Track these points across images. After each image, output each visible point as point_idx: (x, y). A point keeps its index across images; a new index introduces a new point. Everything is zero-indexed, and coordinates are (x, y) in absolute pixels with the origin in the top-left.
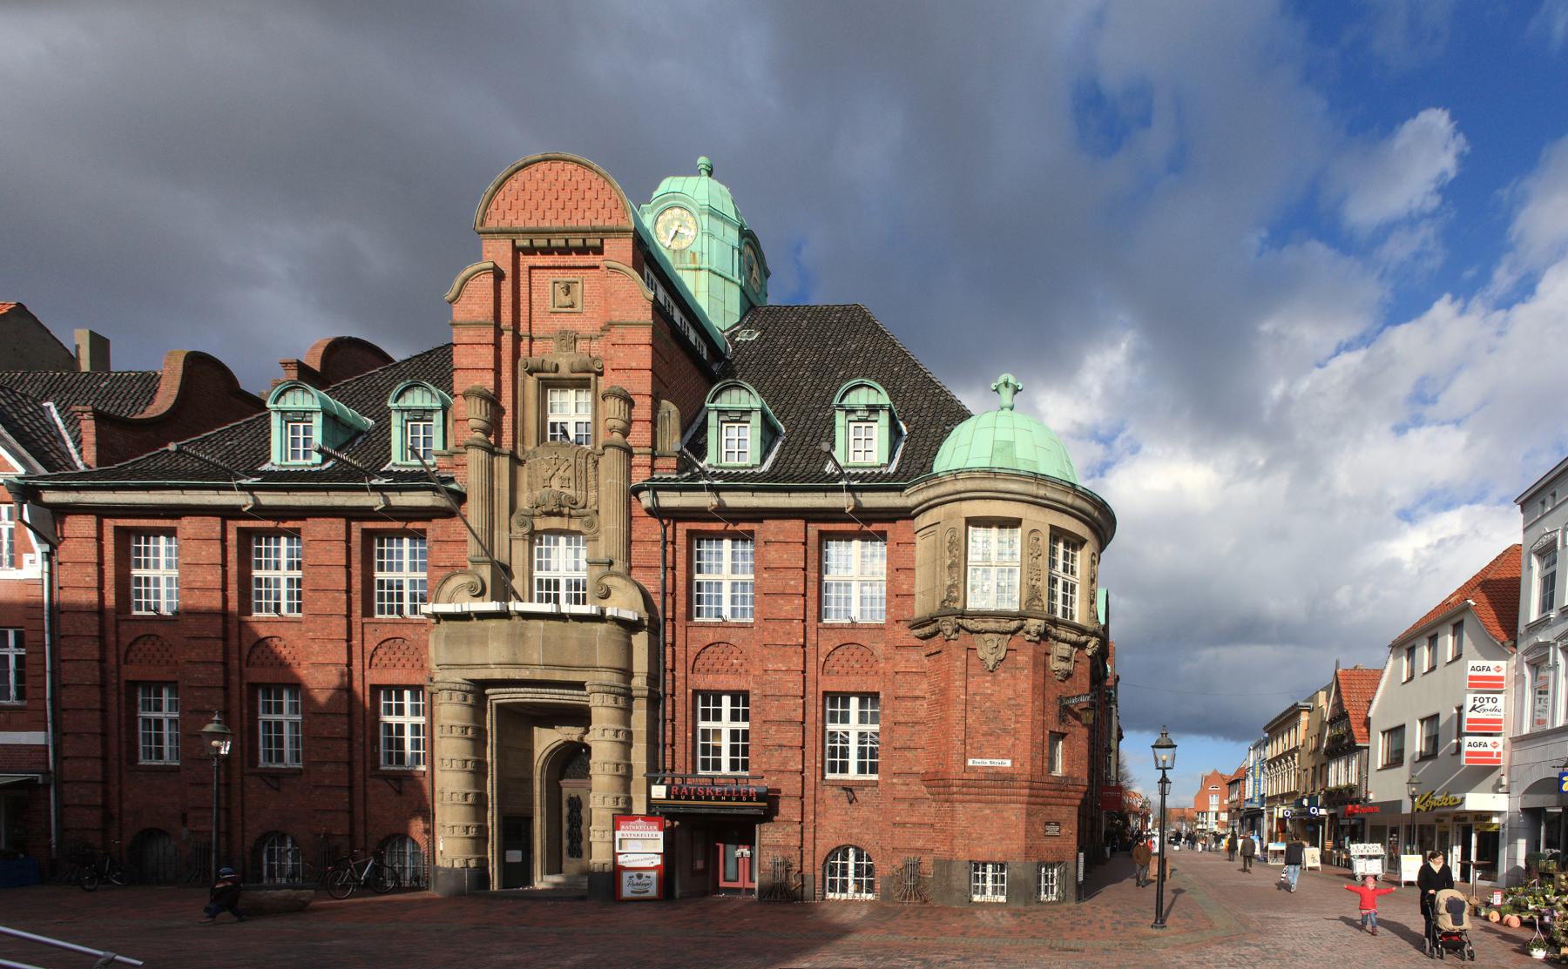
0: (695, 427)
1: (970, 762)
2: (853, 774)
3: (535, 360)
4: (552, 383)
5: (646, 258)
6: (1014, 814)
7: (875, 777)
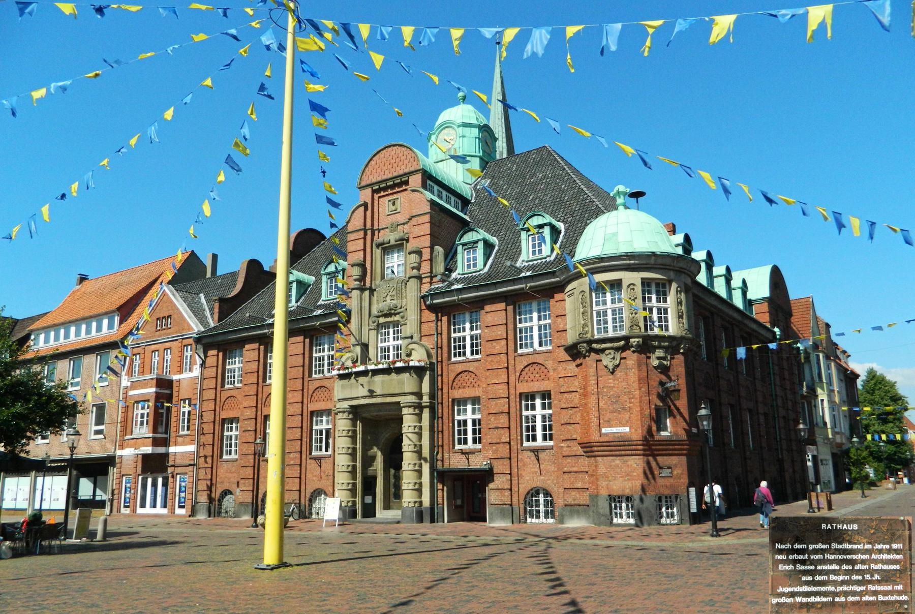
0: (451, 255)
3: (380, 240)
4: (387, 249)
5: (429, 179)
6: (636, 464)
7: (551, 443)
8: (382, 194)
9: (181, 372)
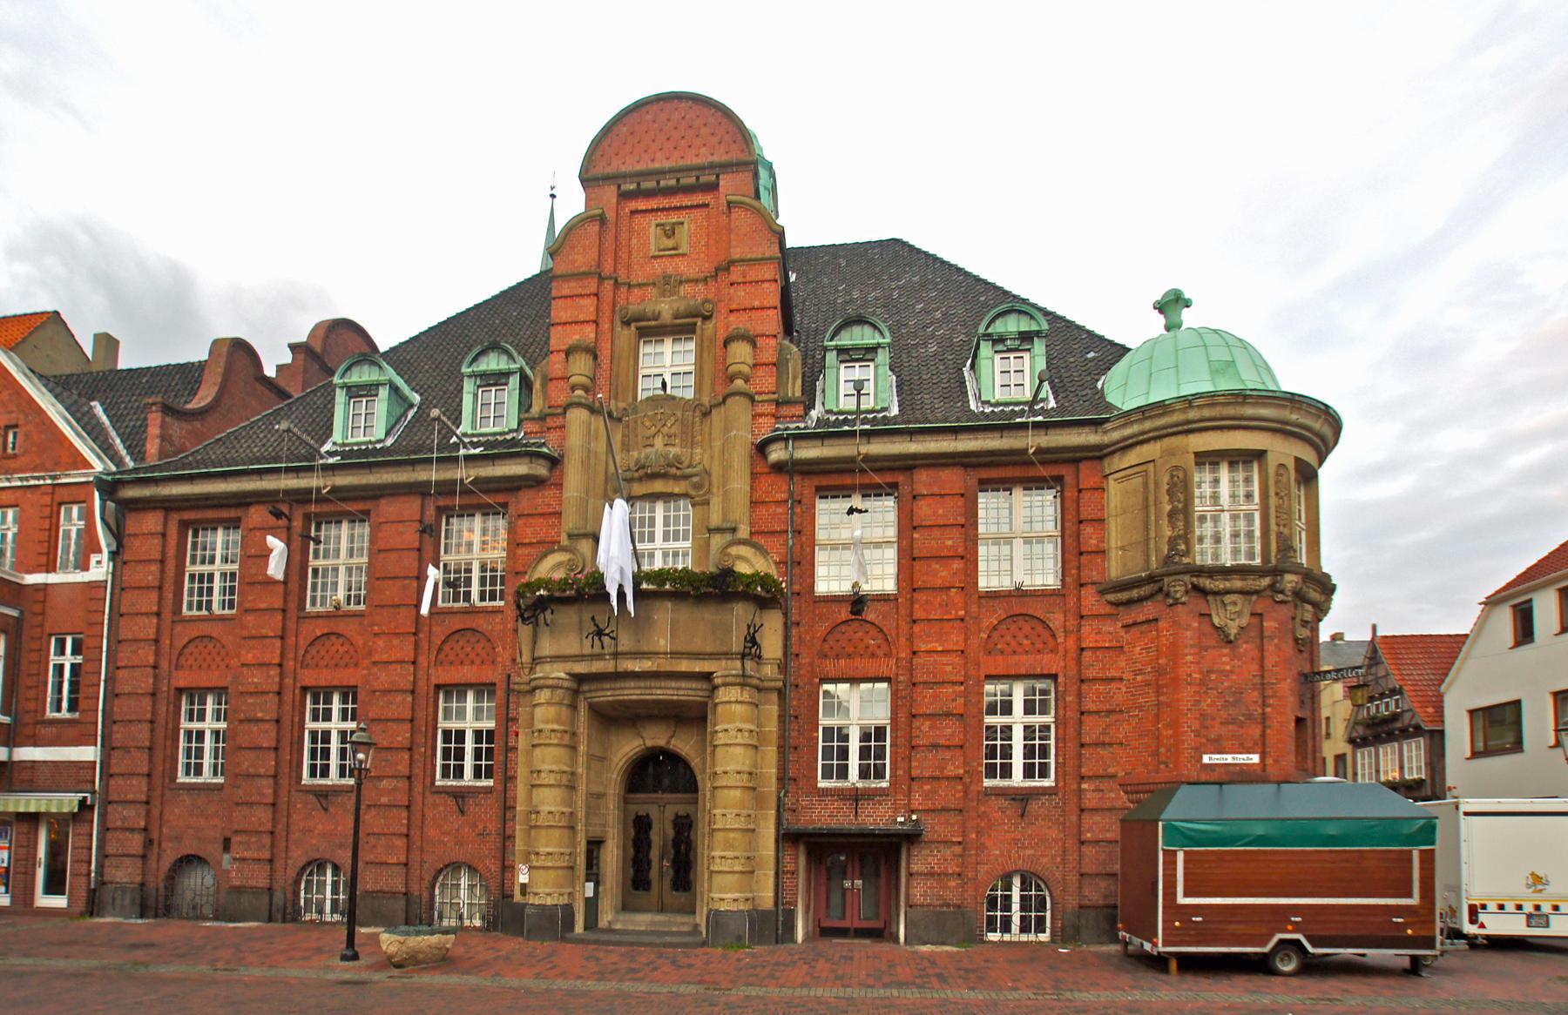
1: (1206, 759)
2: (1017, 778)
3: (634, 308)
8: (641, 205)
9: (50, 568)
